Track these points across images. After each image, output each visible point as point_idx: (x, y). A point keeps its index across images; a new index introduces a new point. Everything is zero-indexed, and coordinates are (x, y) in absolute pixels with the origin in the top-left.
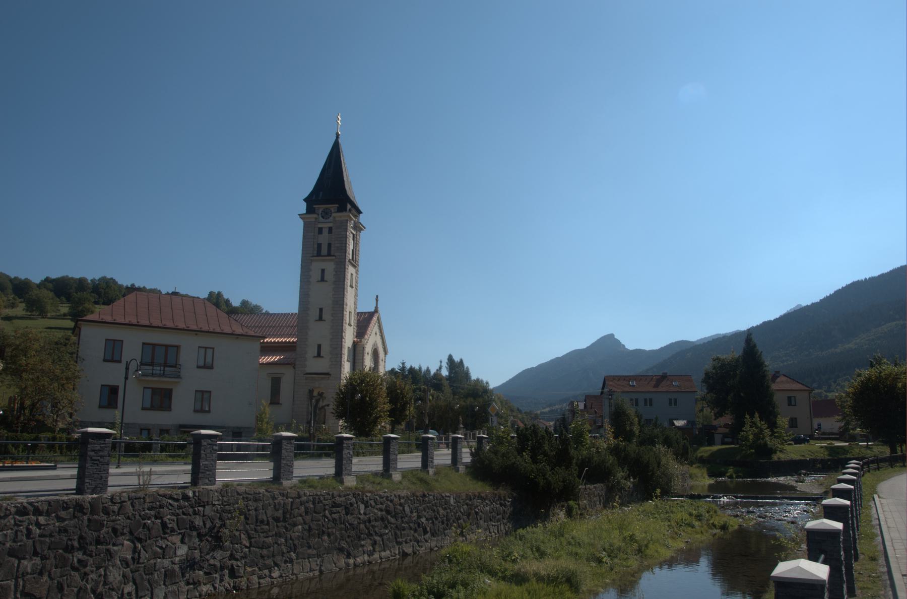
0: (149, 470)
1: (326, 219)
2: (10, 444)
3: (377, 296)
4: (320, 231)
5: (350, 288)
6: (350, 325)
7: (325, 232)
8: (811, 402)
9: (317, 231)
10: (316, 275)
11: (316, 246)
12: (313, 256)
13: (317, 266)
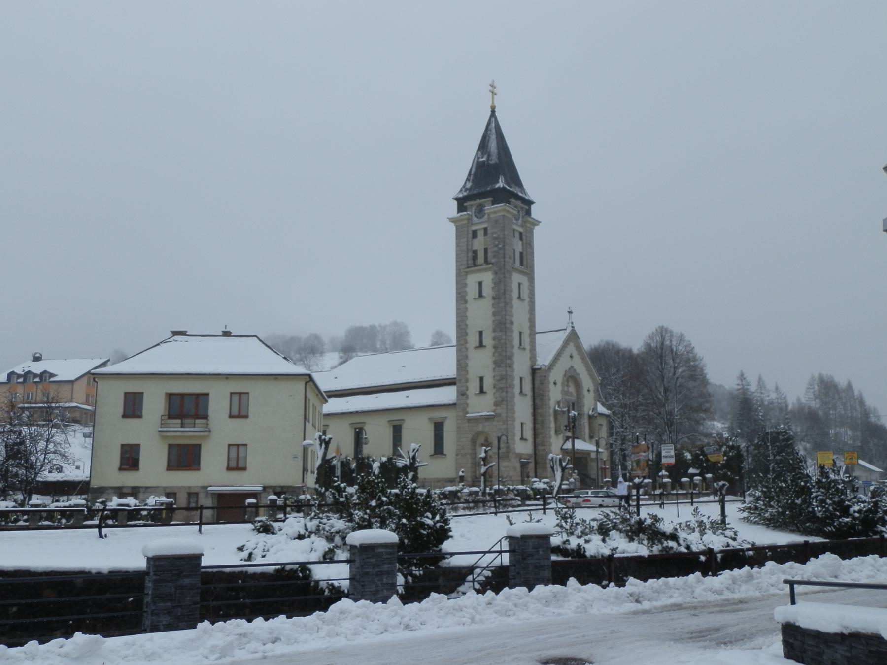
1: (481, 218)
4: (475, 234)
7: (480, 234)
9: (470, 236)
10: (472, 290)
12: (468, 267)
13: (472, 280)
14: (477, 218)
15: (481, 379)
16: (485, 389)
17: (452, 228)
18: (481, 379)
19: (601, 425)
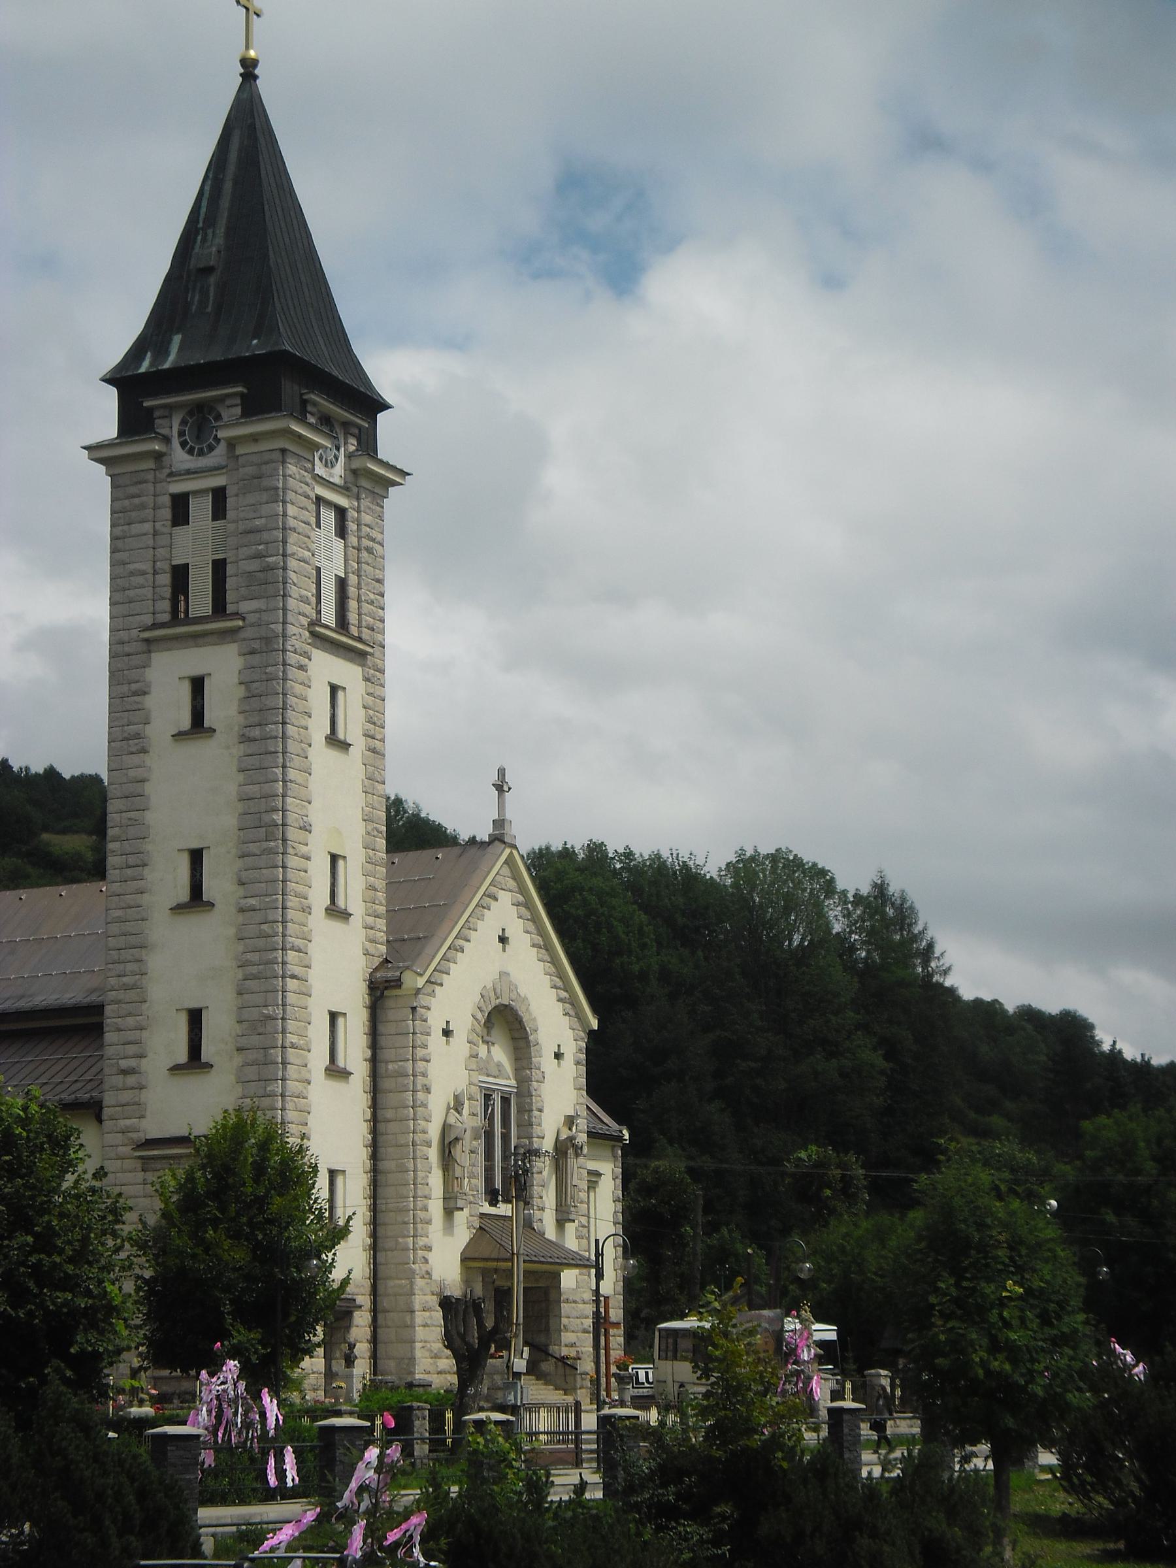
0: (559, 1499)
1: (201, 453)
2: (785, 1387)
3: (501, 772)
4: (180, 510)
5: (333, 754)
6: (335, 911)
7: (200, 509)
8: (337, 630)
9: (166, 513)
11: (165, 579)
12: (155, 626)
14: (191, 452)
15: (195, 1018)
16: (207, 1053)
17: (99, 479)
18: (195, 1018)
19: (598, 1174)
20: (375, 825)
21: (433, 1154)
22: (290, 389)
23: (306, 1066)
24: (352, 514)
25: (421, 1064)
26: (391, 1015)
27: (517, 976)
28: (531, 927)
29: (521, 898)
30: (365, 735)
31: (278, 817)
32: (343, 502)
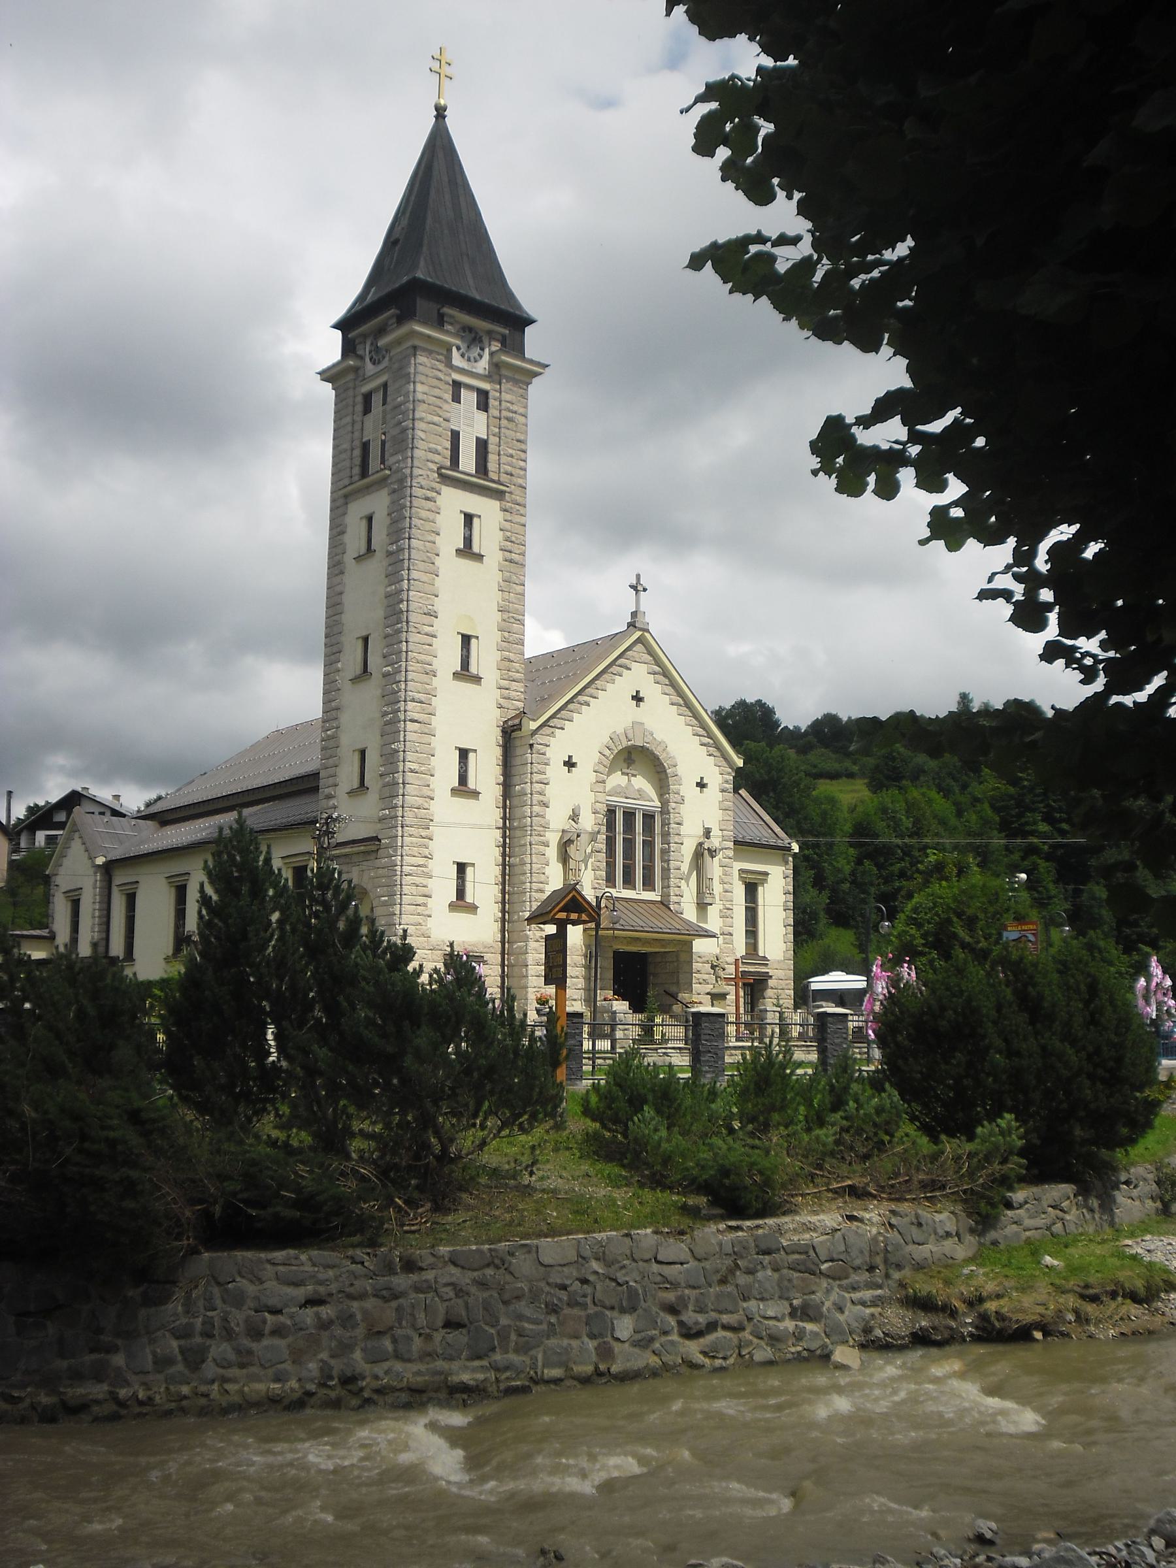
9: (359, 408)
20: (511, 615)
21: (552, 853)
22: (422, 304)
23: (428, 786)
24: (492, 394)
25: (537, 787)
26: (519, 751)
27: (651, 724)
28: (670, 690)
29: (657, 669)
30: (501, 550)
31: (403, 606)
32: (485, 386)
